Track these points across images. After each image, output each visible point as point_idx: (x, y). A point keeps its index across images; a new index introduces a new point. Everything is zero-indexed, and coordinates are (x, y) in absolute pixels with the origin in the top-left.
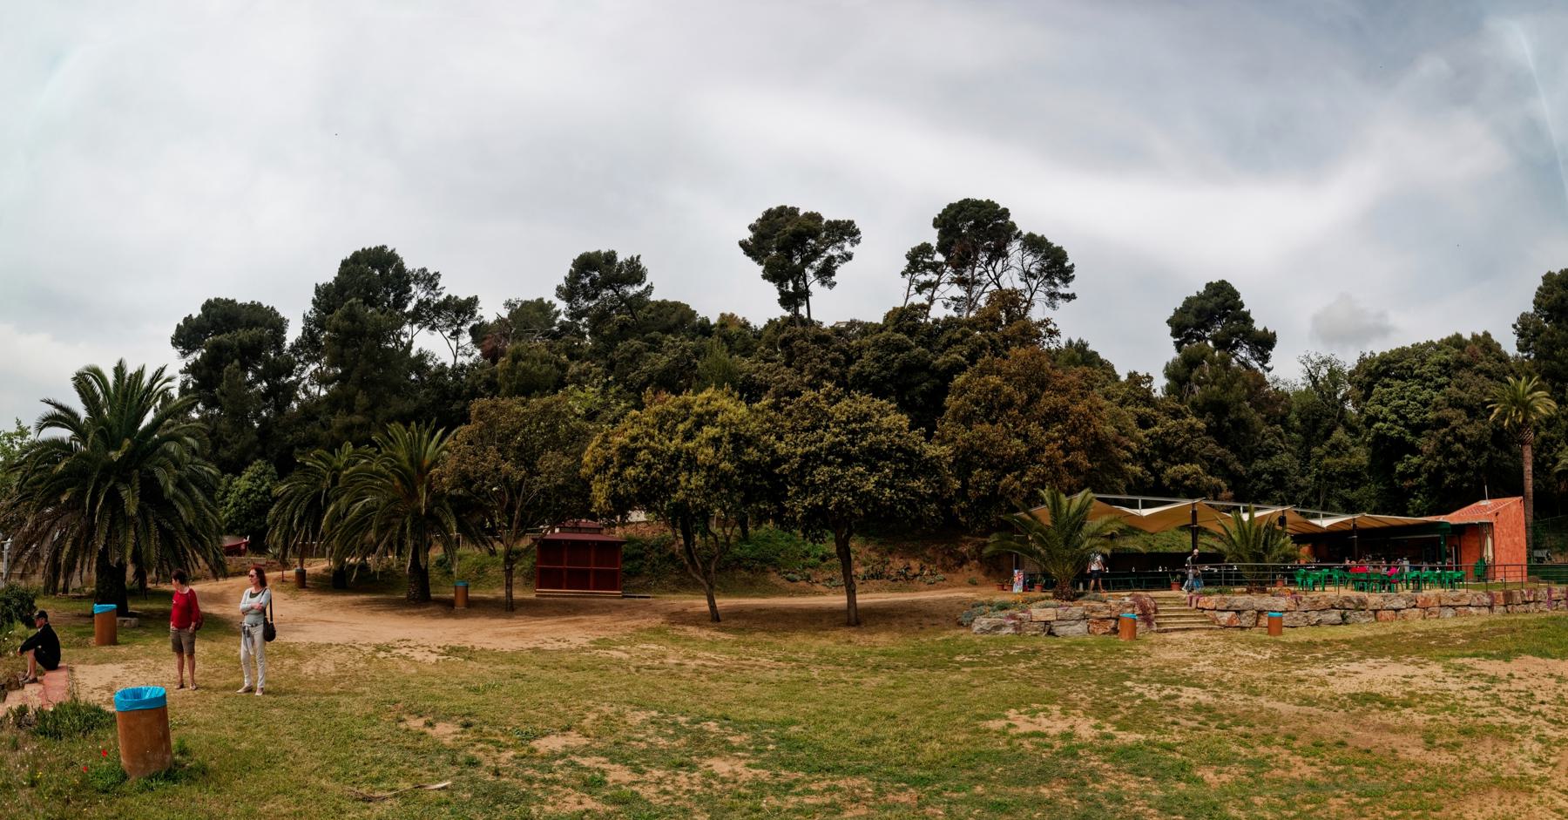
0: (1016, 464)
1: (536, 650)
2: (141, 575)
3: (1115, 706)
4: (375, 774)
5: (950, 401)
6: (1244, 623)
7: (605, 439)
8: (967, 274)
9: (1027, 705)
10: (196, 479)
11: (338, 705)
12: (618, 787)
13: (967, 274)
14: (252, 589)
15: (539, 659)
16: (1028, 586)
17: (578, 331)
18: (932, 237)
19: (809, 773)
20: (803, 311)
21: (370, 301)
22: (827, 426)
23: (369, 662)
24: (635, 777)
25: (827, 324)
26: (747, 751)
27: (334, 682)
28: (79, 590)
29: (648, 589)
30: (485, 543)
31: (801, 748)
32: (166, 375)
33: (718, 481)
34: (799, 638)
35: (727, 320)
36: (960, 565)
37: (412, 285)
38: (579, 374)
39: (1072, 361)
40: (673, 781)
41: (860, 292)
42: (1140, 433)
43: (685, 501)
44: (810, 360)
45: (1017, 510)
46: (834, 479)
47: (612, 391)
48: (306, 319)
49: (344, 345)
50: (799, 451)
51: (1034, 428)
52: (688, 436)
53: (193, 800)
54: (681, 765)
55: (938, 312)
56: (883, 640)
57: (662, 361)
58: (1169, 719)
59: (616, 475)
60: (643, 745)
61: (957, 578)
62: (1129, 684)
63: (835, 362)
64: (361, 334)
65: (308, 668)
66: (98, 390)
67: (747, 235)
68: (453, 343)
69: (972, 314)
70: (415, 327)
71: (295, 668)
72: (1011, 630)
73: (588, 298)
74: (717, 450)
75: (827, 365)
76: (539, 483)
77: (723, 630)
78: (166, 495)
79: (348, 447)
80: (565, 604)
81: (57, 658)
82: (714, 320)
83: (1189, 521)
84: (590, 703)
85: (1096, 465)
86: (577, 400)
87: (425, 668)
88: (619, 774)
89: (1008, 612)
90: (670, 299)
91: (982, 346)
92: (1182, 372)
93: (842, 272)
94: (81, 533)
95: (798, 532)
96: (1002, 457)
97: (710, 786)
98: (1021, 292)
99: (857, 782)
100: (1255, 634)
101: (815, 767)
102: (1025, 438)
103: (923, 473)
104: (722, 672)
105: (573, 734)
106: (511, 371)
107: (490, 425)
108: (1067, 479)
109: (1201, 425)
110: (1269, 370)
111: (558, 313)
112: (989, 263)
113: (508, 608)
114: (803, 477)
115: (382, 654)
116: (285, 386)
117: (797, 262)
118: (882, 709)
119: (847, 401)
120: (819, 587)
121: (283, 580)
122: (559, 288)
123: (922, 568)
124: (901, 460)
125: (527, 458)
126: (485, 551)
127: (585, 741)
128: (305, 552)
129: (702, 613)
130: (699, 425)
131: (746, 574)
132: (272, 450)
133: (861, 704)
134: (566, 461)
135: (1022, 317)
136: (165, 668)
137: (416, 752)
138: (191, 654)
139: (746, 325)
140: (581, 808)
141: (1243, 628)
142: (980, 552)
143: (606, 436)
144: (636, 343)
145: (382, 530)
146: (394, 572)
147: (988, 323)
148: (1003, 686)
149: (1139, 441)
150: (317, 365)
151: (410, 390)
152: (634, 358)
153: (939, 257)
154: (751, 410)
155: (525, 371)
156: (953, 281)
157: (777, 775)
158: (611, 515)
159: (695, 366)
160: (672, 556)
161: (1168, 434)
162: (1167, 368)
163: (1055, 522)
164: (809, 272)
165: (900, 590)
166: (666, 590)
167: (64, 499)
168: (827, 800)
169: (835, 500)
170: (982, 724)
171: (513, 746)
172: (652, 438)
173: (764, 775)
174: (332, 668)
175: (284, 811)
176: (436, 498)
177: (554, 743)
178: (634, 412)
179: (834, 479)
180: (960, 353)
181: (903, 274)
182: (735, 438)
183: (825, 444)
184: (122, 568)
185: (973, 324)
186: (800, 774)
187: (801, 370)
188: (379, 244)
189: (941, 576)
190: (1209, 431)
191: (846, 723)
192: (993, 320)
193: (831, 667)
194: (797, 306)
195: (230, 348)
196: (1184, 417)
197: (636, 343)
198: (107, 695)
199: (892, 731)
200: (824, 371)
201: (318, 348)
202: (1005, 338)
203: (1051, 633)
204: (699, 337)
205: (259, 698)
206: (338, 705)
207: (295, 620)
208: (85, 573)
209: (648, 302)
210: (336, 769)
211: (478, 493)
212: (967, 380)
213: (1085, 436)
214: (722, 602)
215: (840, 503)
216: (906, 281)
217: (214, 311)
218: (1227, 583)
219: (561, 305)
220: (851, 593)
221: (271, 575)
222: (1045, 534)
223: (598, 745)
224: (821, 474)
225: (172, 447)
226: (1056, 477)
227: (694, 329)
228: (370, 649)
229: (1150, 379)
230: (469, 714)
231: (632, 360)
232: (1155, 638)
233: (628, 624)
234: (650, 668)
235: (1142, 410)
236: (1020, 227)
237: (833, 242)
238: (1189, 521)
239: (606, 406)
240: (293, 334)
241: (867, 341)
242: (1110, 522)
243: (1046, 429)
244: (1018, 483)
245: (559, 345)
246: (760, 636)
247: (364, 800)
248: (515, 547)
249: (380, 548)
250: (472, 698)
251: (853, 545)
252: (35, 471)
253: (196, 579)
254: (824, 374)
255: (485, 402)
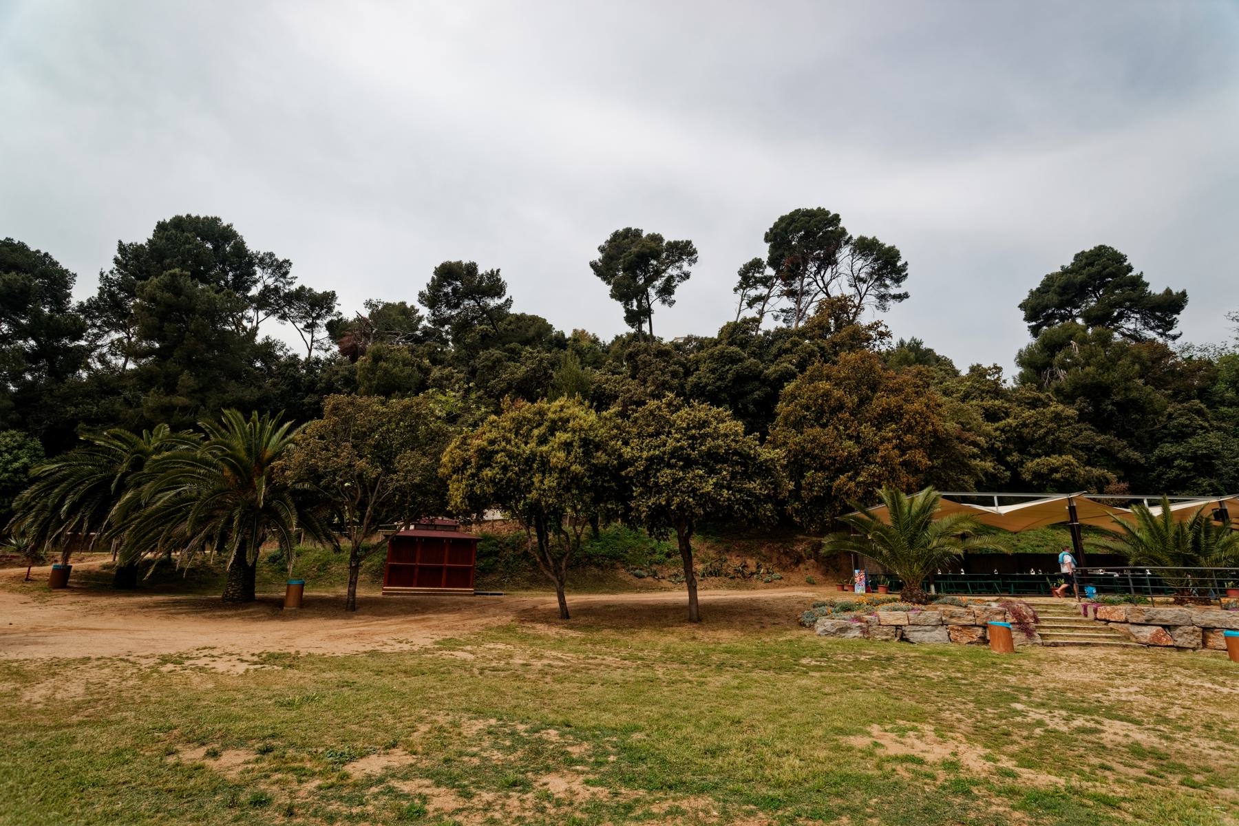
0: (849, 465)
1: (373, 654)
3: (1008, 734)
5: (781, 407)
6: (1180, 642)
7: (464, 442)
8: (797, 285)
9: (892, 721)
11: (73, 740)
13: (797, 285)
15: (374, 663)
16: (871, 586)
17: (440, 337)
18: (763, 252)
19: (650, 791)
20: (645, 327)
22: (670, 433)
23: (144, 678)
24: (460, 803)
25: (667, 340)
26: (587, 764)
27: (77, 708)
29: (501, 585)
31: (642, 759)
33: (570, 482)
35: (579, 336)
36: (797, 564)
38: (442, 378)
39: (905, 361)
41: (697, 310)
42: (989, 427)
43: (538, 501)
44: (652, 372)
45: (852, 510)
46: (676, 481)
47: (473, 396)
50: (645, 454)
51: (867, 430)
52: (543, 441)
54: (514, 784)
55: (769, 324)
56: (726, 637)
57: (521, 371)
58: (1095, 761)
59: (473, 476)
60: (476, 761)
61: (795, 578)
62: (1019, 707)
63: (674, 374)
65: (37, 694)
67: (598, 256)
68: (308, 337)
70: (261, 314)
71: (14, 695)
72: (858, 633)
73: (449, 306)
76: (395, 481)
77: (572, 627)
79: (165, 430)
80: (413, 602)
82: (568, 334)
83: (1065, 518)
84: (424, 712)
85: (937, 463)
86: (438, 404)
87: (228, 681)
89: (853, 614)
90: (529, 313)
91: (812, 354)
92: (1041, 358)
93: (681, 290)
95: (644, 530)
96: (834, 459)
97: (542, 810)
98: (850, 298)
99: (701, 802)
100: (1205, 656)
101: (657, 782)
102: (857, 439)
103: (758, 475)
105: (398, 752)
108: (905, 477)
109: (1071, 411)
110: (1174, 338)
111: (421, 319)
112: (818, 272)
113: (349, 607)
114: (647, 478)
116: (67, 350)
117: (641, 282)
118: (727, 713)
120: (665, 583)
122: (421, 294)
124: (737, 463)
125: (384, 455)
127: (410, 760)
128: (76, 543)
129: (552, 610)
130: (552, 431)
131: (595, 571)
133: (705, 707)
134: (425, 461)
135: (850, 322)
137: (180, 794)
139: (595, 341)
141: (1180, 649)
142: (816, 552)
143: (465, 438)
144: (496, 353)
145: (200, 523)
146: (209, 569)
147: (817, 331)
148: (859, 695)
149: (987, 435)
150: (122, 334)
151: (255, 379)
152: (495, 366)
153: (770, 271)
154: (600, 418)
155: (386, 371)
156: (783, 293)
157: (616, 794)
159: (551, 377)
161: (1024, 425)
162: (1020, 355)
163: (896, 520)
164: (652, 292)
165: (738, 587)
169: (677, 500)
170: (843, 740)
172: (508, 441)
174: (81, 690)
176: (276, 491)
177: (375, 765)
178: (493, 417)
179: (676, 481)
180: (790, 362)
181: (736, 290)
182: (585, 442)
183: (668, 448)
185: (802, 334)
186: (642, 792)
187: (645, 381)
188: (211, 214)
189: (778, 575)
190: (1082, 417)
191: (691, 728)
192: (822, 328)
194: (641, 323)
196: (1045, 405)
197: (496, 353)
199: (737, 739)
200: (664, 383)
201: (125, 314)
202: (834, 345)
203: (903, 639)
204: (555, 350)
207: (34, 629)
209: (508, 315)
211: (326, 488)
213: (923, 434)
214: (573, 599)
216: (738, 297)
218: (1138, 591)
219: (424, 311)
220: (692, 590)
222: (886, 533)
223: (426, 763)
224: (665, 476)
226: (892, 476)
227: (550, 342)
229: (998, 369)
231: (492, 368)
232: (1041, 652)
233: (477, 623)
234: (495, 669)
235: (989, 403)
236: (850, 232)
237: (673, 262)
238: (1065, 518)
239: (467, 410)
240: (83, 291)
241: (703, 354)
242: (962, 520)
243: (879, 429)
246: (608, 633)
248: (365, 543)
249: (194, 542)
251: (693, 543)
254: (664, 386)
255: (343, 398)
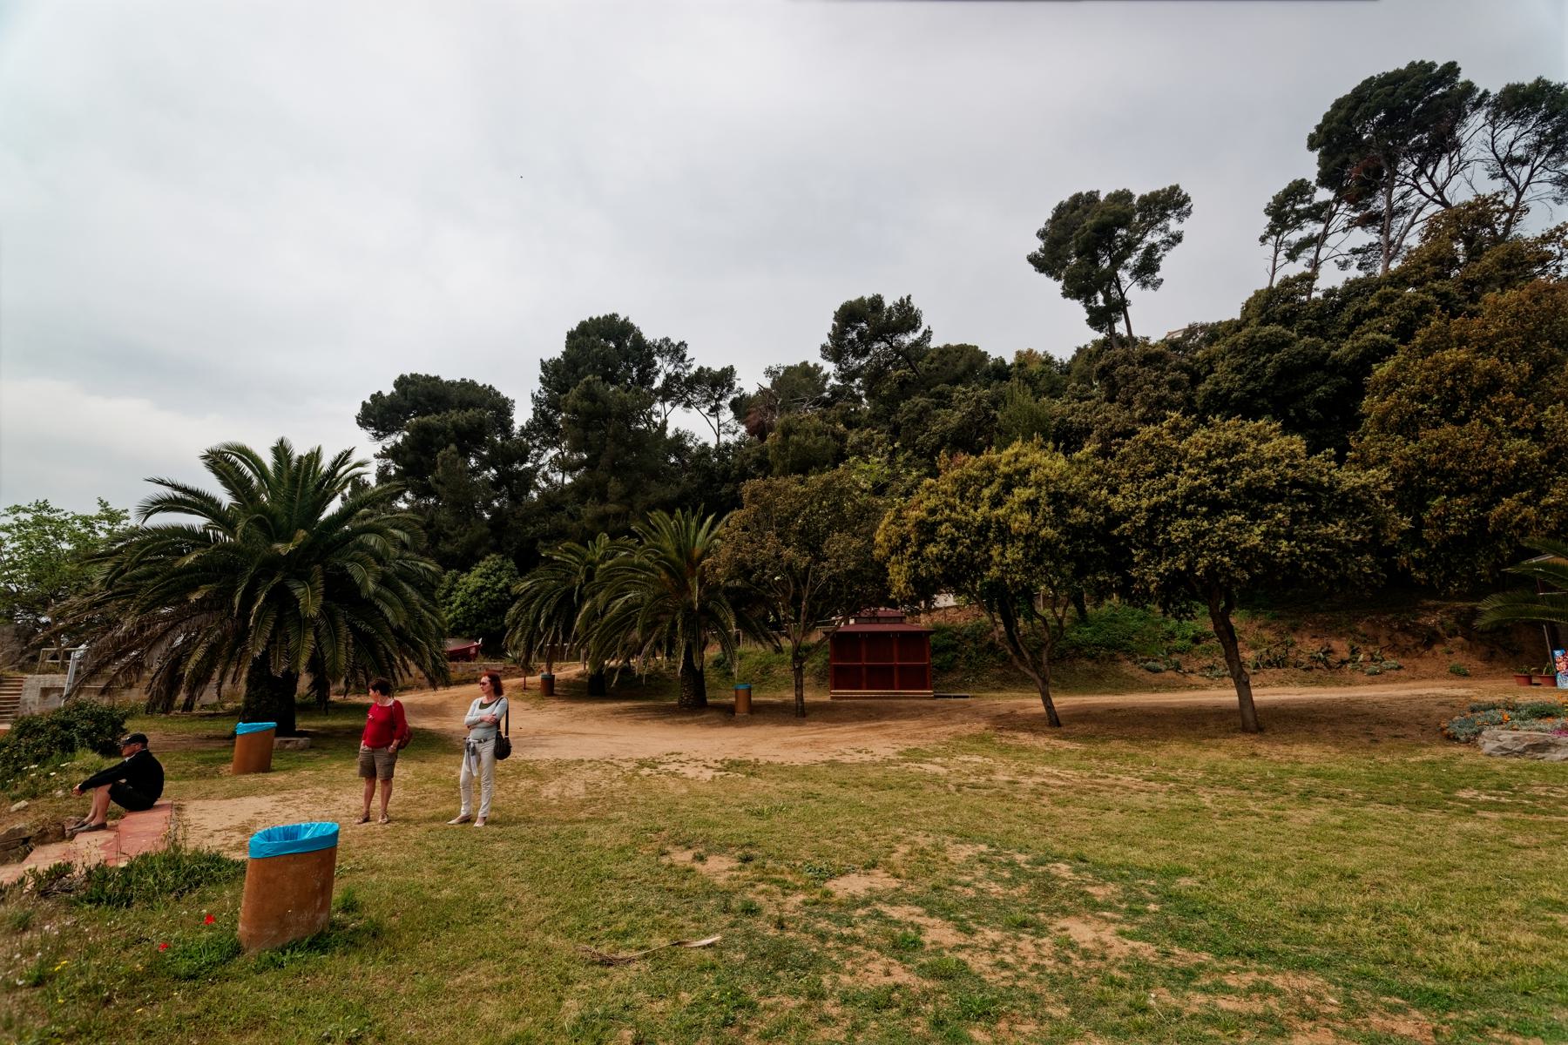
1: (832, 764)
2: (321, 685)
4: (622, 926)
5: (1371, 405)
8: (1379, 203)
10: (407, 576)
11: (584, 835)
12: (938, 952)
14: (484, 699)
18: (1308, 166)
19: (1219, 956)
20: (1120, 328)
21: (610, 378)
22: (1180, 468)
23: (629, 780)
24: (960, 939)
26: (1118, 911)
27: (583, 806)
28: (214, 706)
29: (966, 687)
30: (768, 639)
32: (354, 459)
34: (1175, 748)
35: (1025, 359)
37: (656, 358)
38: (860, 443)
40: (1014, 949)
41: (1195, 288)
43: (1002, 579)
44: (1140, 388)
47: (901, 459)
48: (535, 399)
49: (586, 427)
50: (1145, 503)
52: (997, 502)
53: (346, 976)
54: (1023, 925)
55: (1331, 278)
56: (1309, 754)
59: (915, 555)
60: (971, 892)
61: (1424, 666)
63: (1175, 385)
64: (607, 415)
65: (550, 791)
66: (248, 472)
67: (1037, 245)
68: (714, 421)
69: (1394, 266)
70: (668, 405)
71: (534, 791)
73: (858, 355)
74: (1035, 514)
75: (1165, 391)
76: (827, 570)
77: (1065, 737)
78: (364, 594)
79: (604, 539)
80: (866, 707)
81: (157, 791)
84: (900, 831)
86: (862, 474)
87: (698, 787)
88: (939, 933)
90: (954, 343)
91: (1424, 308)
93: (1169, 263)
94: (224, 638)
95: (1156, 608)
96: (1490, 473)
97: (1067, 961)
99: (1307, 982)
103: (1341, 512)
104: (1071, 794)
105: (879, 873)
106: (783, 447)
107: (766, 508)
111: (827, 377)
112: (1421, 170)
113: (798, 713)
114: (1153, 535)
115: (646, 771)
117: (1105, 266)
118: (1328, 860)
119: (1205, 431)
120: (1194, 678)
121: (525, 688)
122: (824, 348)
123: (1354, 652)
124: (1300, 499)
125: (812, 542)
126: (770, 648)
127: (895, 883)
128: (554, 655)
130: (1008, 488)
131: (1089, 665)
132: (510, 544)
134: (856, 543)
136: (344, 799)
138: (388, 779)
139: (1049, 360)
140: (889, 981)
143: (899, 511)
144: (920, 401)
145: (648, 629)
146: (663, 675)
147: (1429, 269)
150: (556, 451)
152: (921, 418)
153: (1323, 195)
154: (1071, 462)
155: (798, 445)
156: (1352, 224)
157: (1168, 954)
158: (913, 601)
159: (995, 418)
160: (992, 647)
164: (1124, 275)
165: (1319, 682)
166: (987, 687)
167: (193, 598)
168: (1259, 1008)
169: (1203, 562)
171: (803, 888)
172: (953, 508)
173: (1147, 951)
175: (486, 983)
176: (711, 591)
178: (928, 481)
179: (1199, 535)
180: (1381, 330)
181: (1263, 240)
182: (1055, 498)
183: (1180, 490)
184: (291, 678)
185: (1400, 280)
186: (1205, 957)
188: (609, 313)
193: (1231, 792)
194: (1112, 324)
195: (443, 431)
197: (920, 401)
198: (238, 837)
199: (1355, 902)
201: (556, 431)
205: (478, 830)
206: (584, 835)
207: (538, 733)
208: (227, 685)
209: (928, 350)
210: (571, 920)
211: (758, 583)
212: (1398, 367)
214: (1062, 701)
215: (1213, 564)
216: (1269, 248)
217: (412, 388)
219: (829, 367)
220: (1243, 686)
221: (508, 683)
223: (912, 889)
224: (1180, 529)
225: (372, 540)
227: (987, 374)
228: (632, 765)
230: (750, 845)
231: (918, 421)
234: (974, 786)
237: (1152, 225)
239: (896, 476)
240: (522, 416)
241: (1217, 347)
244: (1530, 511)
245: (833, 413)
247: (601, 963)
248: (805, 643)
249: (646, 648)
250: (754, 824)
252: (139, 563)
253: (406, 689)
255: (758, 483)
